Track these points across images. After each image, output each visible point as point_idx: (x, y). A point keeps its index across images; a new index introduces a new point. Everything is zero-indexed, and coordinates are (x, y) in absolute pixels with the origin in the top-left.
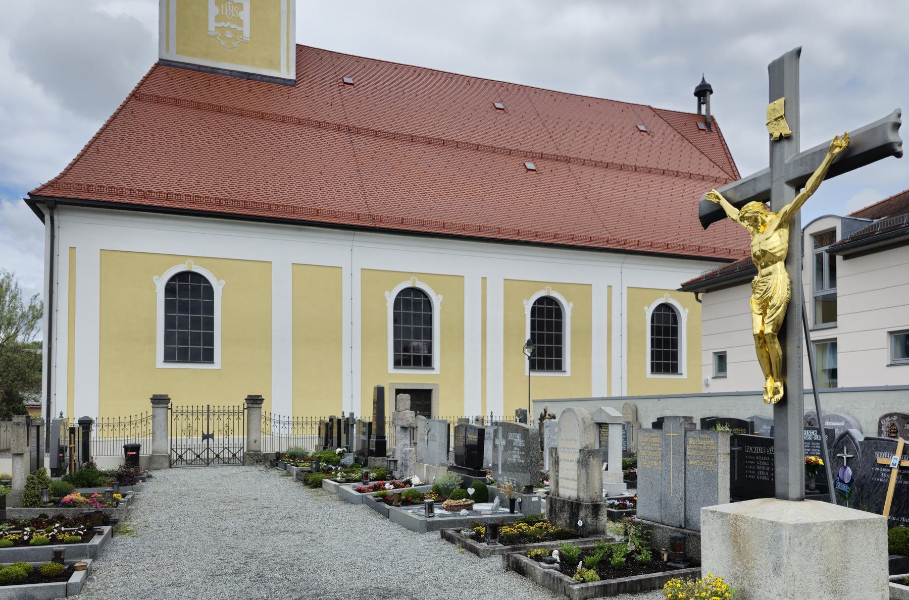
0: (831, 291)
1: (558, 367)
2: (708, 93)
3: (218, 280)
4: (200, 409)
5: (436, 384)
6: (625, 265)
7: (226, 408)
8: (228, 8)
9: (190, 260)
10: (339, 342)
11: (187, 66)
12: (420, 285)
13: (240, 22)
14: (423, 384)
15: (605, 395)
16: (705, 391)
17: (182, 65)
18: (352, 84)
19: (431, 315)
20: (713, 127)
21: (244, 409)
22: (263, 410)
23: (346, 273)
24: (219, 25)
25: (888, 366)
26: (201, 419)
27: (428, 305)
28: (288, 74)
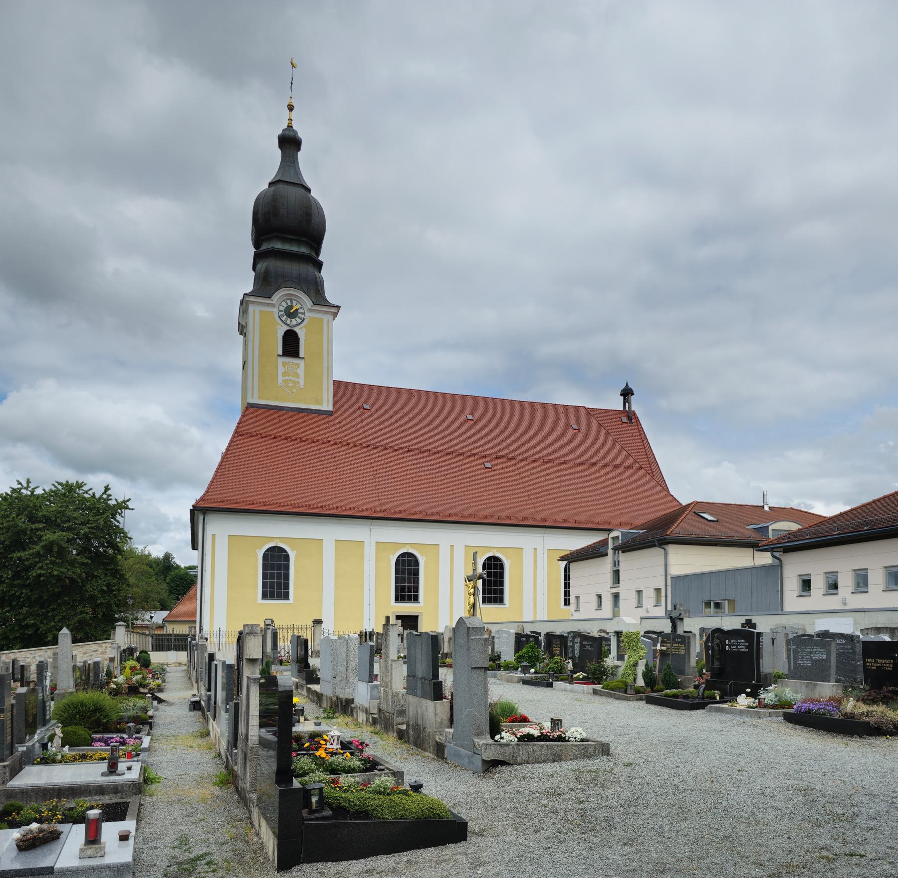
0: (618, 569)
1: (501, 601)
6: (545, 535)
9: (277, 540)
10: (362, 587)
13: (297, 376)
14: (412, 612)
15: (532, 619)
16: (571, 618)
17: (262, 406)
18: (369, 410)
20: (633, 421)
22: (322, 627)
24: (284, 379)
27: (417, 563)
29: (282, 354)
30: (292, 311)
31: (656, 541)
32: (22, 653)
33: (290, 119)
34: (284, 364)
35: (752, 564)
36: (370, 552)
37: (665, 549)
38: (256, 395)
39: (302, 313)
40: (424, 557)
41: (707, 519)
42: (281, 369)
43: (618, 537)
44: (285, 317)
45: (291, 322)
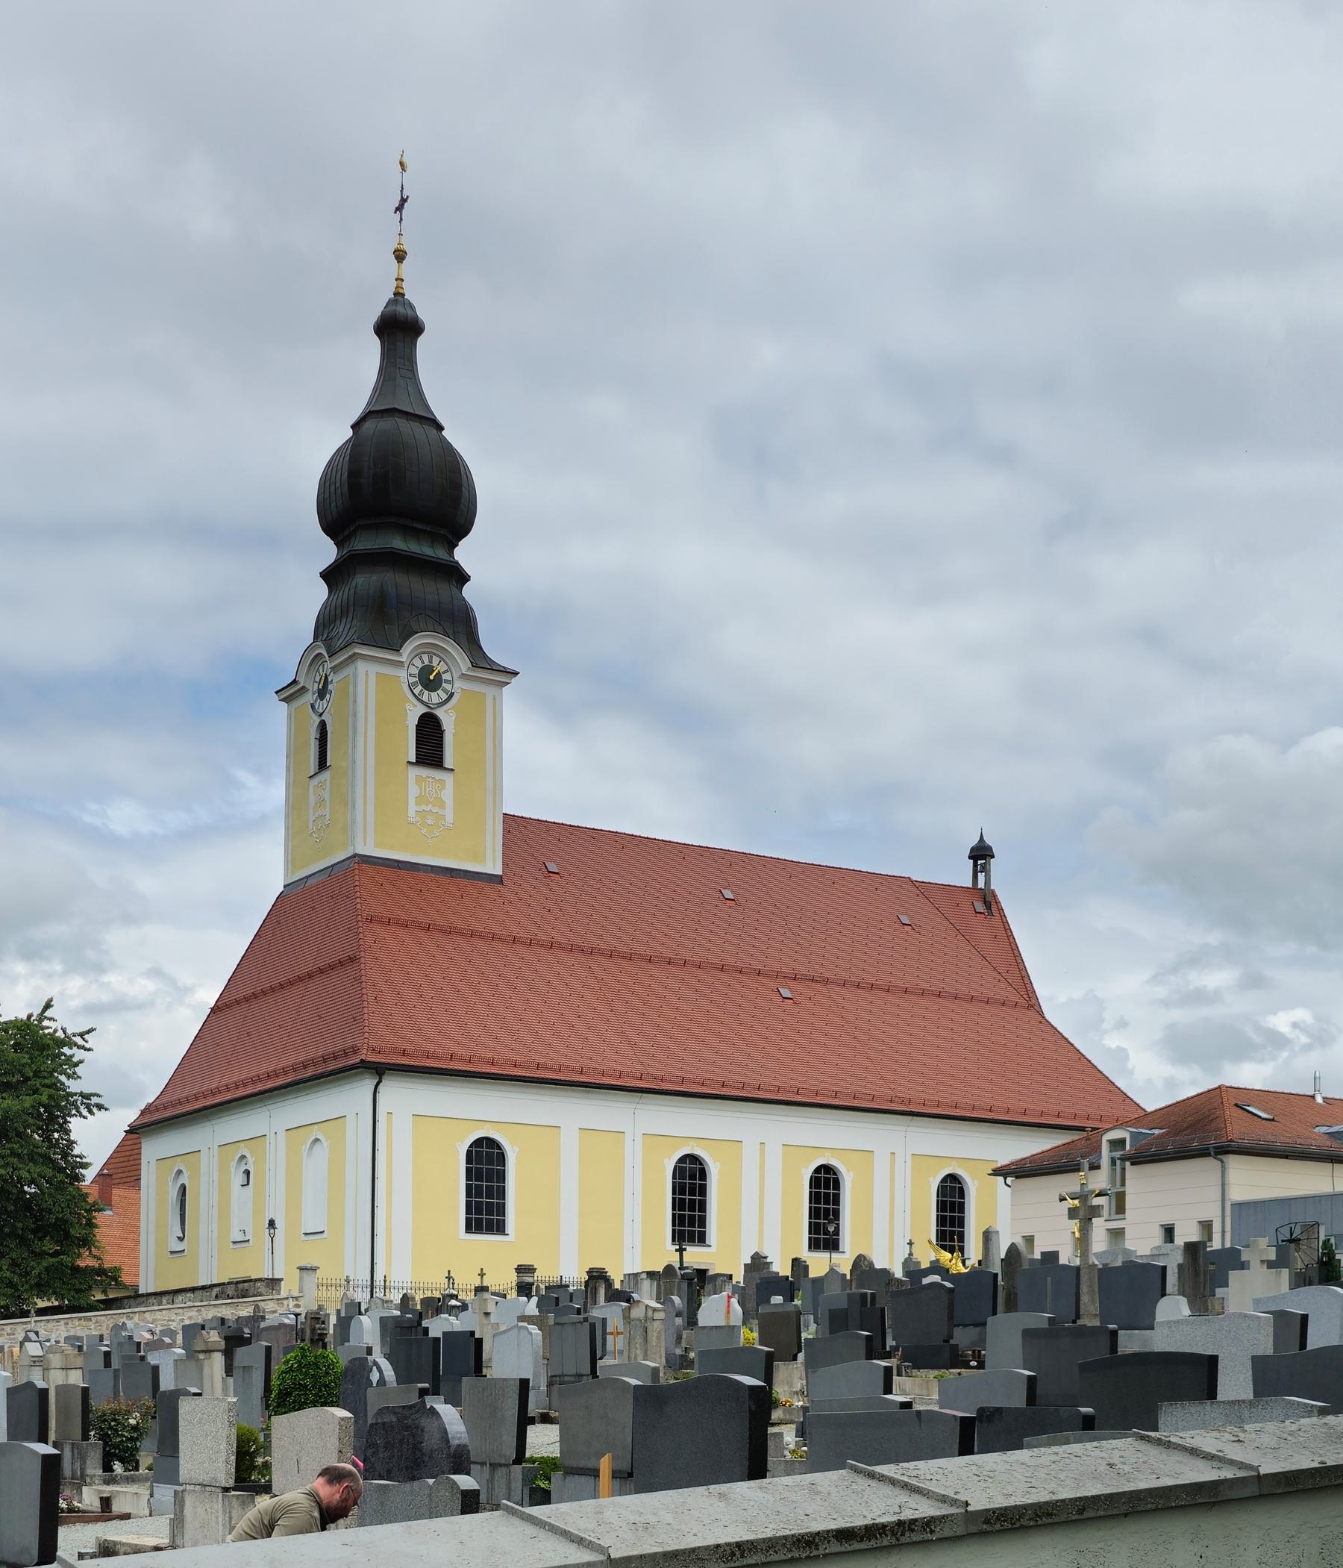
6: (910, 1129)
9: (488, 1125)
12: (698, 1151)
13: (442, 804)
23: (628, 1138)
28: (494, 867)
29: (414, 760)
30: (432, 677)
31: (1211, 1149)
32: (164, 1312)
33: (399, 279)
35: (1332, 1190)
36: (633, 1152)
37: (1222, 1162)
40: (718, 1164)
41: (1260, 1117)
42: (413, 790)
43: (1122, 1141)
44: (420, 687)
45: (430, 697)
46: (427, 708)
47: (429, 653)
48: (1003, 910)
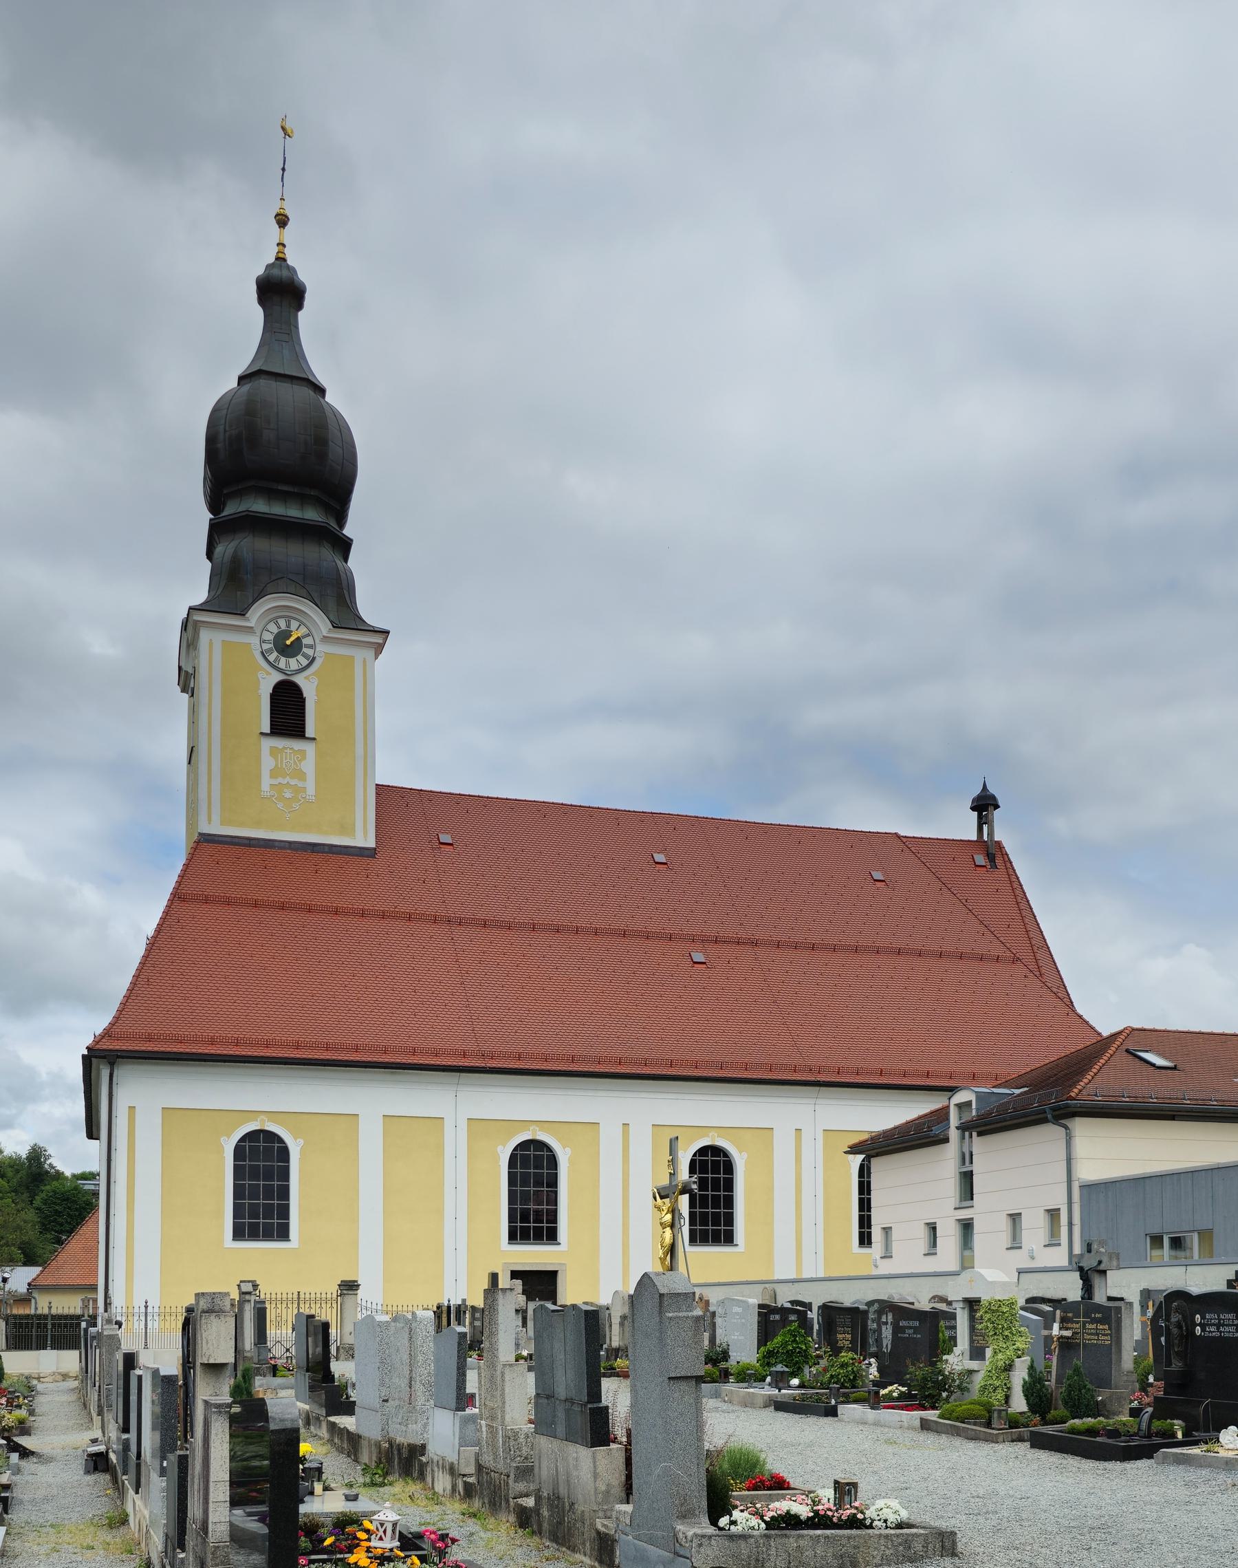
0: (969, 1169)
2: (990, 808)
3: (295, 1139)
4: (290, 1296)
5: (564, 1264)
6: (819, 1101)
7: (318, 1295)
8: (286, 759)
9: (263, 1117)
10: (440, 1212)
11: (234, 840)
12: (542, 1137)
13: (302, 776)
14: (545, 1264)
15: (793, 1276)
17: (229, 839)
19: (557, 1173)
20: (999, 861)
21: (337, 1296)
22: (359, 1297)
25: (1045, 1246)
26: (291, 1308)
30: (288, 642)
33: (283, 245)
34: (274, 752)
36: (455, 1140)
37: (1066, 1128)
38: (216, 817)
39: (310, 647)
41: (1153, 1065)
42: (268, 763)
43: (969, 1104)
44: (275, 654)
45: (287, 664)
46: (281, 674)
47: (288, 617)
48: (1011, 863)
